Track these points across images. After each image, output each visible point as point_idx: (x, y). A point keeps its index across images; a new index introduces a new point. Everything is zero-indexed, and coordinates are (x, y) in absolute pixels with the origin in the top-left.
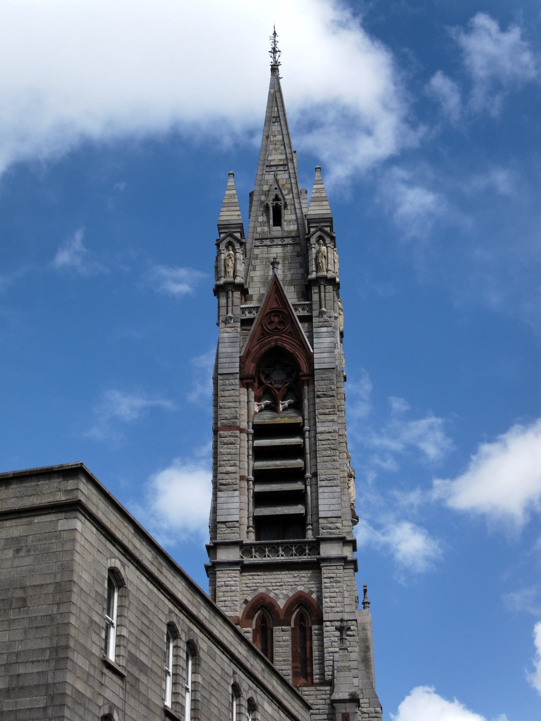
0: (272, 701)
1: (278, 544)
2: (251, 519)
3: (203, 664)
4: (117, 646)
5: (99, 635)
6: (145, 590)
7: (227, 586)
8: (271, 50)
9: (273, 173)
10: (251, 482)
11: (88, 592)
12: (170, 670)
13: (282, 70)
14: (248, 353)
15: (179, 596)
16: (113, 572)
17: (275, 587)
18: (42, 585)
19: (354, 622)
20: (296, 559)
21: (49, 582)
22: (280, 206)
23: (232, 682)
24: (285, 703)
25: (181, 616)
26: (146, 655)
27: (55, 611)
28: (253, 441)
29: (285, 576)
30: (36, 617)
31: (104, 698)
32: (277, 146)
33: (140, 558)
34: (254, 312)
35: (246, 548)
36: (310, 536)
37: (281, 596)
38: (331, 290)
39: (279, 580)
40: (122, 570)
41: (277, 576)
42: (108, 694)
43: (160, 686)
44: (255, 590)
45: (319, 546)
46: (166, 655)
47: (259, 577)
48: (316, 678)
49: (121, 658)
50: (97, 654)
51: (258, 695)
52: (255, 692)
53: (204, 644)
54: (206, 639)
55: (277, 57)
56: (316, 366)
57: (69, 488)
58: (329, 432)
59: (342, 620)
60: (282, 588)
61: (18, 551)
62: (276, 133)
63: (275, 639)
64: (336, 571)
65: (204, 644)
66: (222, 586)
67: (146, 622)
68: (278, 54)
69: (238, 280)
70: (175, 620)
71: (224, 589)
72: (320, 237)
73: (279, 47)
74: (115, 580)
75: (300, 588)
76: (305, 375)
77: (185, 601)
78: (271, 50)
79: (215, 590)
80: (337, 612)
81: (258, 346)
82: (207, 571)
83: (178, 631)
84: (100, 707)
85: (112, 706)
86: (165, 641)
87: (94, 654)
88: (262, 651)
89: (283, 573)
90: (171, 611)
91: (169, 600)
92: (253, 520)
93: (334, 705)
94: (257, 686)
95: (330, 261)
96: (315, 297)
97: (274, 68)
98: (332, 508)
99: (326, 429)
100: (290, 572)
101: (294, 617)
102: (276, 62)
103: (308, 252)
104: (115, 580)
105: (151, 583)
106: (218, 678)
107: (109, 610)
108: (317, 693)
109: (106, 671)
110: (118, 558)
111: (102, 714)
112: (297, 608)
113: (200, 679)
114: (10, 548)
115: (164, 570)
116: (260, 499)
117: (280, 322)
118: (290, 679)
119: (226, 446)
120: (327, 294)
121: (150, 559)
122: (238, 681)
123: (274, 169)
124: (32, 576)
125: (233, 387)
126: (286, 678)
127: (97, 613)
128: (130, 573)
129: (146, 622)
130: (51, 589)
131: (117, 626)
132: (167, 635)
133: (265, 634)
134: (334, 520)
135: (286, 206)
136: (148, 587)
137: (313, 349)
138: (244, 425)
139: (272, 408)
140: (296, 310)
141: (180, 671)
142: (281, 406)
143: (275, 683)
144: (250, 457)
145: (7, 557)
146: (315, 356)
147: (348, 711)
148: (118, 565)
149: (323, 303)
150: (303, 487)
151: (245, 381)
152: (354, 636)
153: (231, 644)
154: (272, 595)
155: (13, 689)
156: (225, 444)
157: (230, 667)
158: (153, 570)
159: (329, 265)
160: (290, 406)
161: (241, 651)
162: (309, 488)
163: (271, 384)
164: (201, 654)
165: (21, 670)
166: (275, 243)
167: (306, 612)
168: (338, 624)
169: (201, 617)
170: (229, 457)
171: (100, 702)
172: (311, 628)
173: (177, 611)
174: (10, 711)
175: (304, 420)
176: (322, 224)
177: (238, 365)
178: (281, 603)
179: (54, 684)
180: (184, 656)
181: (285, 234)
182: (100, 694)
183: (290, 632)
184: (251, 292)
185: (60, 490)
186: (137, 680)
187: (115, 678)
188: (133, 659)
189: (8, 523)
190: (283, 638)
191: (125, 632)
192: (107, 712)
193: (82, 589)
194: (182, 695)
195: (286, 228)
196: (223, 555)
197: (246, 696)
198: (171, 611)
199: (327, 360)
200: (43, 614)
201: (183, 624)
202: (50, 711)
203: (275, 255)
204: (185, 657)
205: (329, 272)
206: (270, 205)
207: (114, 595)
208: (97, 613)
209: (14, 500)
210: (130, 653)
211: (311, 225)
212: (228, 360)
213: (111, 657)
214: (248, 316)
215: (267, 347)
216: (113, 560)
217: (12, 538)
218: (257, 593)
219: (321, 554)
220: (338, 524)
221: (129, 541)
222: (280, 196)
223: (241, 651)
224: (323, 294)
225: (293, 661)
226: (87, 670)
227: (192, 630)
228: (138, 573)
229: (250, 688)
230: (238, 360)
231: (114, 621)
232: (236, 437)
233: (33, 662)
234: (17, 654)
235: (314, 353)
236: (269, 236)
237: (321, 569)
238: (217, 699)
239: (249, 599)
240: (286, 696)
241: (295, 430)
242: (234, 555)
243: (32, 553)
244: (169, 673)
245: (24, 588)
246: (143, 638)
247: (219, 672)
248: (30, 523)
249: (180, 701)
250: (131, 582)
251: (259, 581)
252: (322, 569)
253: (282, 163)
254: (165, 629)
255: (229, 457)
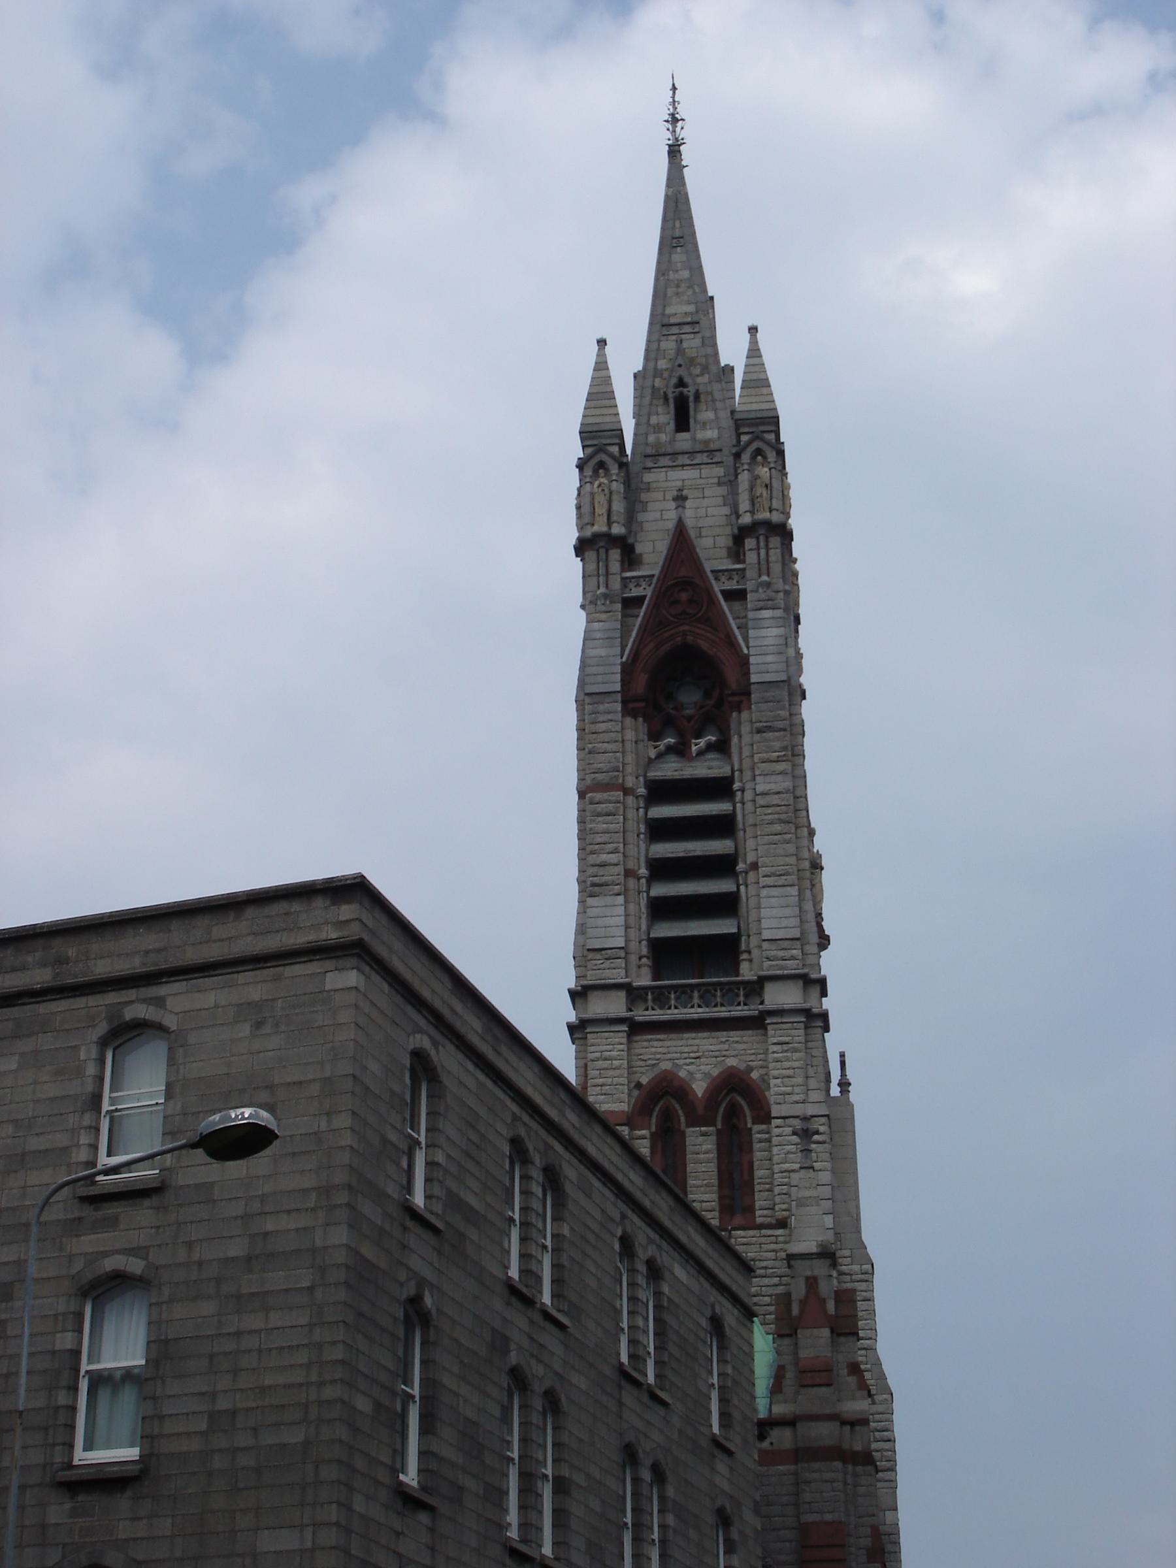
0: (687, 1261)
1: (692, 987)
2: (644, 943)
3: (570, 1205)
4: (428, 1180)
5: (397, 1164)
6: (472, 1084)
7: (606, 1059)
8: (667, 117)
9: (674, 337)
10: (643, 881)
11: (377, 1092)
12: (517, 1217)
13: (687, 154)
14: (636, 655)
15: (529, 1091)
16: (419, 1056)
17: (688, 1061)
18: (301, 1083)
19: (823, 1120)
20: (722, 1012)
21: (311, 1077)
22: (688, 397)
23: (619, 1233)
24: (710, 1264)
25: (534, 1125)
26: (476, 1194)
27: (324, 1125)
28: (646, 810)
29: (706, 1042)
30: (291, 1136)
31: (409, 1269)
32: (680, 290)
33: (463, 1030)
34: (644, 585)
35: (634, 994)
36: (747, 972)
37: (698, 1076)
38: (779, 545)
39: (695, 1048)
40: (433, 1053)
41: (690, 1042)
42: (415, 1262)
43: (501, 1246)
44: (654, 1065)
45: (762, 988)
46: (510, 1192)
47: (661, 1043)
48: (761, 1216)
49: (434, 1200)
50: (395, 1196)
51: (664, 1254)
52: (659, 1247)
53: (571, 1170)
54: (575, 1161)
55: (678, 129)
56: (754, 678)
57: (342, 918)
58: (778, 793)
59: (806, 1119)
60: (699, 1061)
61: (259, 1025)
62: (679, 265)
63: (689, 1149)
64: (793, 1032)
65: (571, 1170)
66: (597, 1059)
67: (474, 1137)
68: (680, 124)
69: (617, 530)
70: (523, 1133)
71: (600, 1064)
72: (758, 452)
73: (682, 112)
74: (422, 1067)
75: (732, 1062)
76: (733, 694)
77: (538, 1100)
78: (667, 117)
79: (586, 1066)
80: (797, 1102)
81: (652, 645)
82: (571, 1034)
83: (527, 1150)
84: (401, 1285)
85: (422, 1283)
86: (507, 1168)
87: (389, 1196)
88: (664, 1171)
89: (700, 1035)
90: (515, 1118)
91: (513, 1099)
92: (648, 946)
93: (792, 1262)
94: (662, 1237)
95: (775, 493)
96: (751, 557)
97: (674, 151)
98: (785, 923)
99: (774, 787)
100: (714, 1034)
101: (722, 1110)
102: (677, 140)
103: (736, 477)
104: (422, 1067)
105: (482, 1070)
106: (595, 1227)
107: (414, 1126)
108: (763, 1240)
109: (409, 1223)
110: (426, 1033)
111: (404, 1296)
112: (727, 1095)
113: (566, 1231)
114: (246, 1021)
115: (504, 1049)
116: (661, 909)
117: (691, 601)
118: (714, 1221)
119: (600, 819)
120: (772, 552)
121: (480, 1031)
122: (629, 1230)
123: (675, 330)
124: (284, 1067)
125: (610, 717)
126: (707, 1215)
127: (393, 1127)
128: (448, 1059)
129: (474, 1137)
130: (315, 1089)
131: (427, 1146)
132: (511, 1158)
133: (669, 1139)
134: (786, 944)
135: (697, 397)
136: (476, 1078)
137: (748, 647)
138: (630, 782)
139: (680, 750)
140: (717, 579)
141: (533, 1219)
142: (694, 748)
143: (691, 1230)
144: (642, 836)
145: (241, 1035)
146: (752, 660)
147: (816, 1273)
148: (426, 1044)
149: (764, 568)
150: (733, 888)
151: (631, 705)
152: (823, 1142)
153: (617, 1168)
154: (682, 1074)
155: (257, 1257)
156: (599, 815)
157: (615, 1208)
158: (485, 1048)
159: (774, 501)
160: (710, 747)
161: (633, 1180)
162: (742, 888)
163: (675, 709)
164: (569, 1188)
165: (270, 1226)
166: (679, 462)
167: (743, 1103)
168: (797, 1123)
169: (566, 1125)
170: (605, 838)
171: (402, 1276)
172: (750, 1129)
173: (526, 1118)
174: (252, 1294)
175: (733, 771)
176: (762, 428)
177: (618, 677)
178: (699, 1088)
179: (326, 1248)
180: (538, 1191)
181: (698, 447)
182: (401, 1263)
183: (714, 1138)
184: (639, 549)
185: (327, 923)
186: (462, 1236)
187: (426, 1235)
188: (455, 1202)
189: (241, 978)
190: (701, 1148)
191: (440, 1158)
192: (413, 1292)
193: (368, 1088)
194: (536, 1257)
195: (700, 435)
196: (600, 1006)
197: (643, 1254)
198: (515, 1118)
199: (773, 667)
200: (304, 1132)
201: (535, 1138)
202: (318, 1294)
203: (679, 484)
204: (540, 1195)
205: (774, 513)
206: (671, 396)
207: (420, 1095)
208: (393, 1127)
209: (250, 938)
210: (449, 1192)
211: (742, 430)
212: (601, 669)
213: (419, 1200)
214: (635, 592)
215: (667, 647)
216: (418, 1036)
217: (249, 1004)
218: (656, 1071)
219: (766, 1002)
220: (794, 952)
221: (444, 1002)
222: (687, 379)
223: (633, 1180)
224: (763, 552)
225: (720, 1186)
226: (379, 1223)
227: (552, 1148)
228: (460, 1056)
229: (651, 1241)
230: (619, 668)
231: (422, 1139)
232: (619, 802)
233: (289, 1212)
234: (263, 1198)
235: (748, 656)
236: (669, 450)
237: (766, 1029)
238: (595, 1261)
239: (644, 1080)
240: (710, 1251)
241: (721, 788)
242: (615, 1005)
243: (282, 1028)
244: (514, 1221)
245: (270, 1087)
246: (471, 1166)
247: (597, 1214)
248: (277, 979)
249: (534, 1268)
250: (449, 1072)
251: (660, 1050)
252: (769, 1027)
253: (689, 319)
254: (506, 1149)
255: (605, 838)
